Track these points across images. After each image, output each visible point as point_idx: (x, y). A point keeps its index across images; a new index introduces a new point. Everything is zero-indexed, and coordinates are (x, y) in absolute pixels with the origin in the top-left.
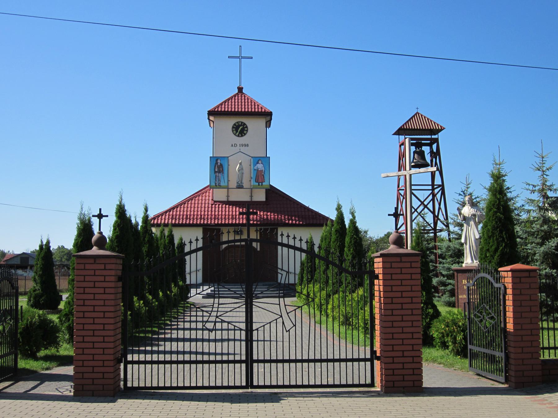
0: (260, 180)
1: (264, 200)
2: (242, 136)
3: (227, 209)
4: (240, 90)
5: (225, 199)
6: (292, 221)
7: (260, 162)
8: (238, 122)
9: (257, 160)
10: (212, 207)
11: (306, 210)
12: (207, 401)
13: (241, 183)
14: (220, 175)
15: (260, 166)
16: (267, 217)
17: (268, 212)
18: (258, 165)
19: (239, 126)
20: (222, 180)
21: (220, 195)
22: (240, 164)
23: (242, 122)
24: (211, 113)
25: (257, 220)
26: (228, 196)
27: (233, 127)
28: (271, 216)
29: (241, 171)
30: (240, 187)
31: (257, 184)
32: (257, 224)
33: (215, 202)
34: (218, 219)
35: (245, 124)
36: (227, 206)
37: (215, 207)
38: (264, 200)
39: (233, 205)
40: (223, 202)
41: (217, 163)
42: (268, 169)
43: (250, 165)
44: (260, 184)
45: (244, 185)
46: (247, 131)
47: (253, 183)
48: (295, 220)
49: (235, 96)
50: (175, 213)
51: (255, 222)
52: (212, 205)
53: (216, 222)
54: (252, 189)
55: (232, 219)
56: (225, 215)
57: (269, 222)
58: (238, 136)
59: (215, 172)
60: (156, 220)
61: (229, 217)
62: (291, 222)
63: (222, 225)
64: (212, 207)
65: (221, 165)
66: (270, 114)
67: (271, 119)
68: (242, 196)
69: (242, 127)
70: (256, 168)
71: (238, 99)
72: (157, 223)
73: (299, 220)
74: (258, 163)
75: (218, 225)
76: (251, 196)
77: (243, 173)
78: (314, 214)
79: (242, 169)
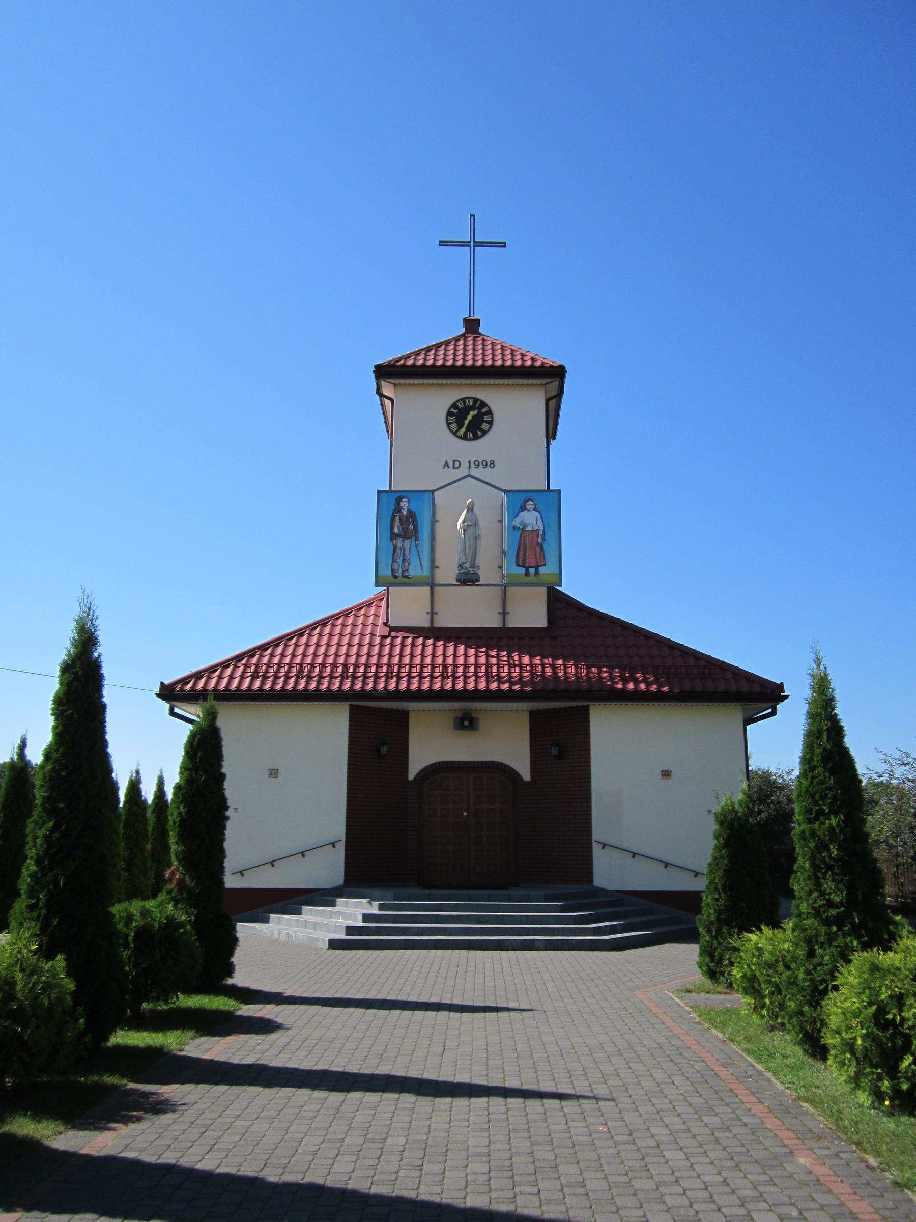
0: (531, 560)
1: (543, 623)
2: (476, 437)
3: (429, 650)
4: (472, 325)
5: (423, 621)
6: (648, 684)
7: (530, 505)
8: (463, 400)
9: (522, 499)
10: (382, 645)
11: (678, 653)
12: (426, 1010)
13: (473, 565)
14: (407, 543)
15: (530, 518)
16: (555, 672)
17: (555, 658)
18: (524, 514)
19: (467, 410)
20: (414, 562)
21: (410, 607)
22: (470, 509)
23: (476, 400)
24: (384, 372)
25: (521, 681)
26: (432, 613)
27: (449, 414)
28: (568, 670)
29: (470, 531)
30: (468, 579)
31: (522, 571)
32: (510, 690)
33: (393, 629)
34: (399, 678)
35: (483, 404)
36: (430, 641)
37: (392, 645)
38: (543, 623)
39: (447, 639)
40: (416, 632)
41: (398, 509)
42: (554, 524)
43: (501, 522)
44: (532, 571)
45: (481, 573)
46: (491, 423)
47: (511, 569)
48: (645, 680)
49: (457, 339)
50: (265, 660)
51: (516, 687)
52: (384, 637)
53: (392, 686)
54: (505, 586)
55: (444, 677)
56: (422, 665)
57: (563, 687)
58: (465, 438)
59: (394, 536)
60: (203, 681)
61: (433, 672)
62: (631, 686)
63: (410, 696)
64: (382, 645)
65: (411, 513)
66: (557, 373)
67: (561, 391)
68: (473, 610)
69: (475, 412)
70: (517, 522)
71: (465, 350)
72: (215, 689)
73: (656, 681)
74: (523, 508)
75: (397, 695)
76: (504, 613)
77: (477, 538)
78: (691, 662)
79: (476, 525)
